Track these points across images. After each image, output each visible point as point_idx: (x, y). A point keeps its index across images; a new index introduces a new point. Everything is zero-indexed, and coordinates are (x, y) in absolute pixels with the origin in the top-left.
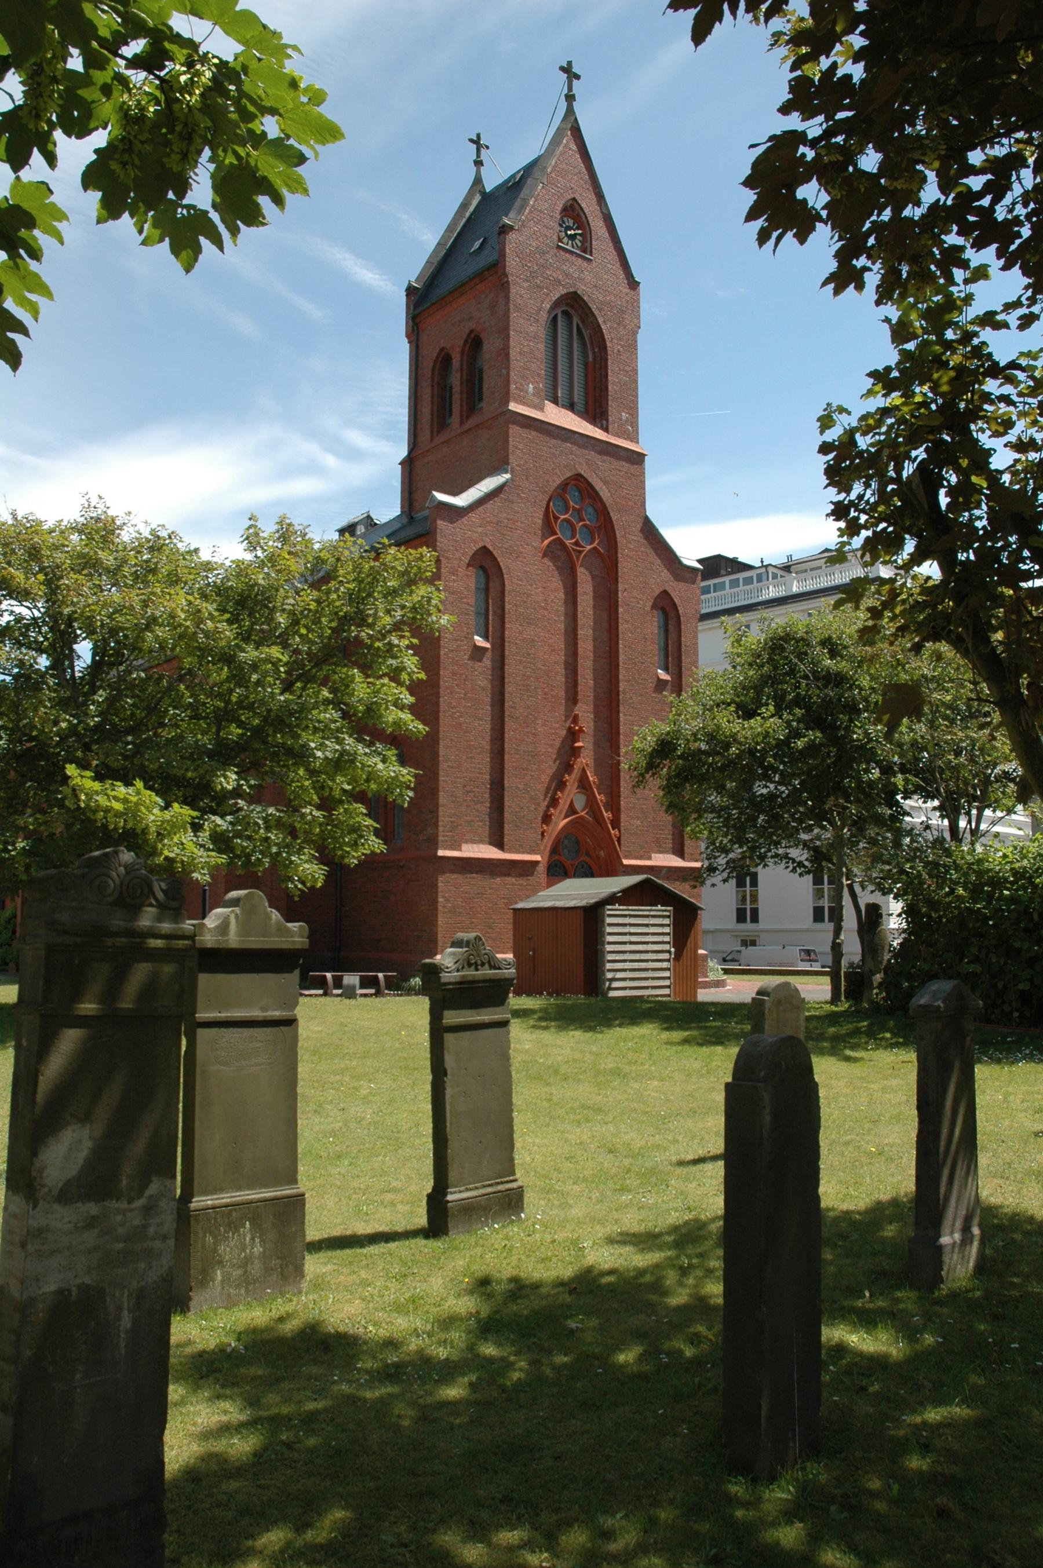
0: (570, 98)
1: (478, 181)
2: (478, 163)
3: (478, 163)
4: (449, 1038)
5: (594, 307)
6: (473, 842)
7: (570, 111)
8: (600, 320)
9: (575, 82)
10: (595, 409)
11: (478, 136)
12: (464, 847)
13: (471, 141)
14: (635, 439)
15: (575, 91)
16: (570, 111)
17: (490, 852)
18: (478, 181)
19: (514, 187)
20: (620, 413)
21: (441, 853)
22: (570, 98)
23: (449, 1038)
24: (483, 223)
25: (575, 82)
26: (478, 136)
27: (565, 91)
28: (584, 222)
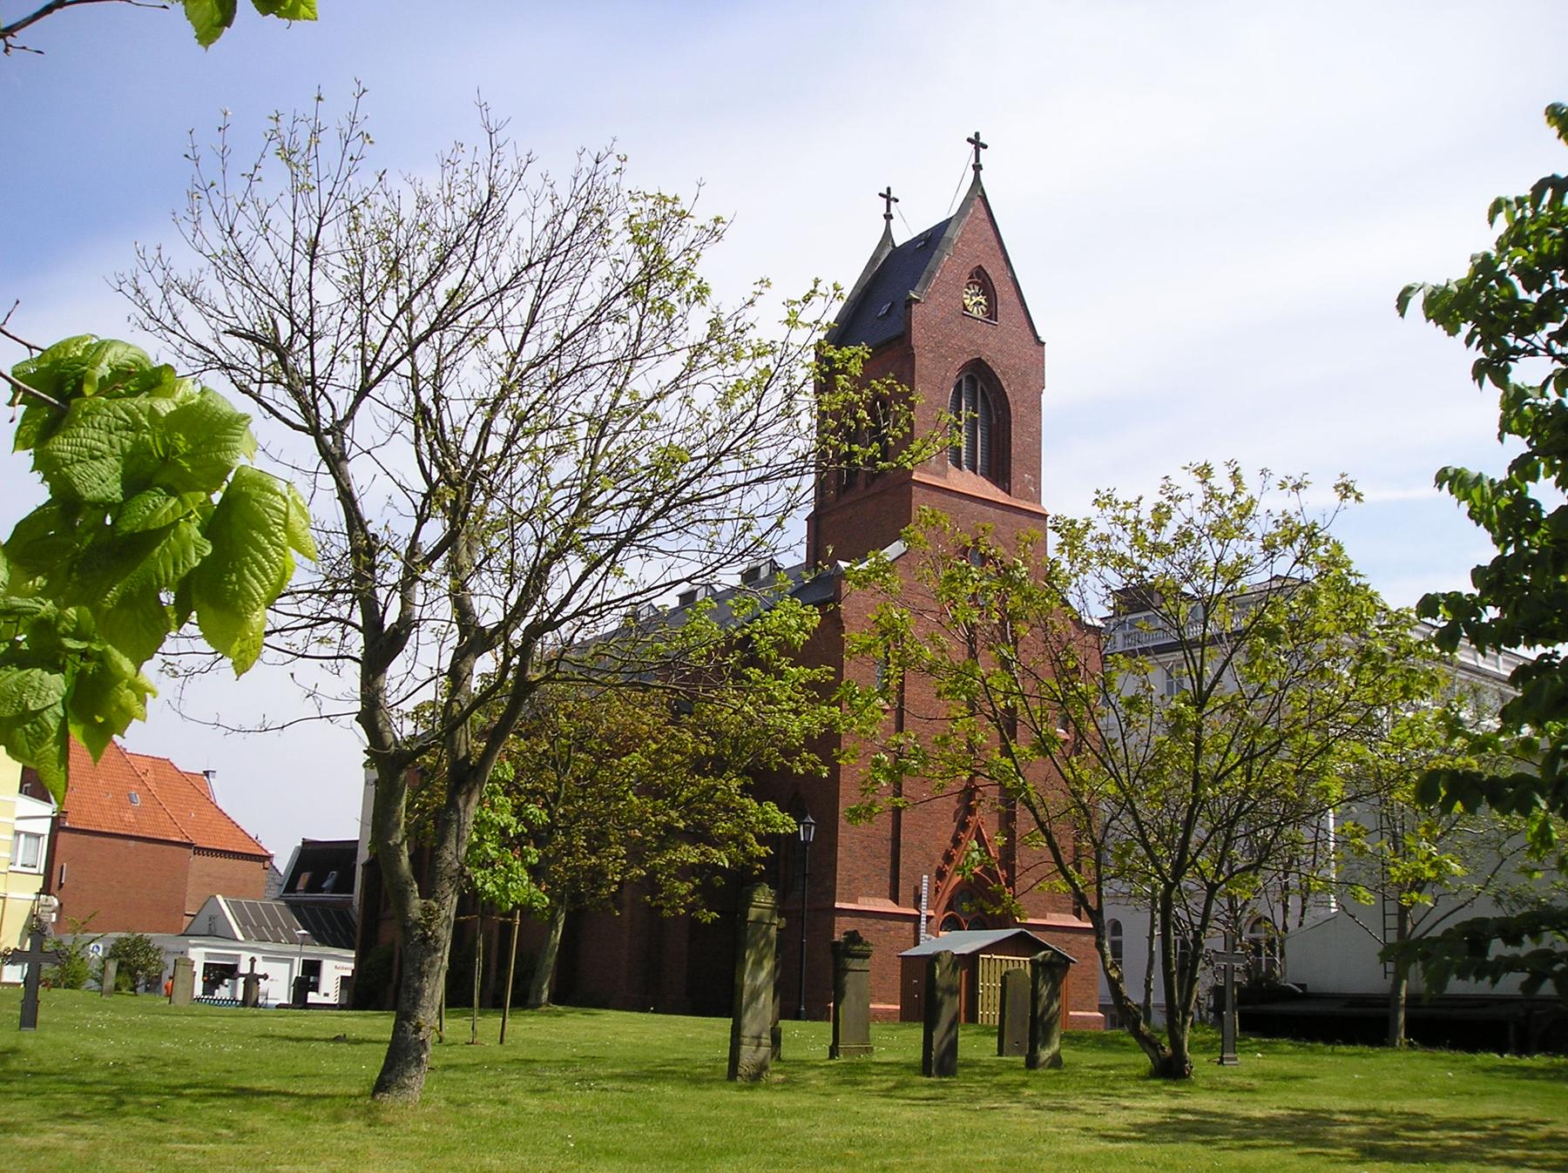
0: (977, 168)
1: (888, 234)
2: (888, 217)
3: (888, 217)
4: (62, 836)
5: (998, 372)
6: (869, 895)
7: (977, 181)
8: (1004, 384)
9: (982, 151)
10: (999, 471)
11: (977, 135)
12: (860, 900)
13: (969, 140)
14: (1037, 498)
15: (892, 211)
16: (977, 181)
17: (888, 906)
18: (888, 234)
19: (931, 240)
20: (1022, 474)
21: (837, 905)
22: (977, 168)
23: (62, 836)
24: (896, 274)
25: (982, 151)
26: (977, 135)
27: (973, 161)
28: (994, 283)
